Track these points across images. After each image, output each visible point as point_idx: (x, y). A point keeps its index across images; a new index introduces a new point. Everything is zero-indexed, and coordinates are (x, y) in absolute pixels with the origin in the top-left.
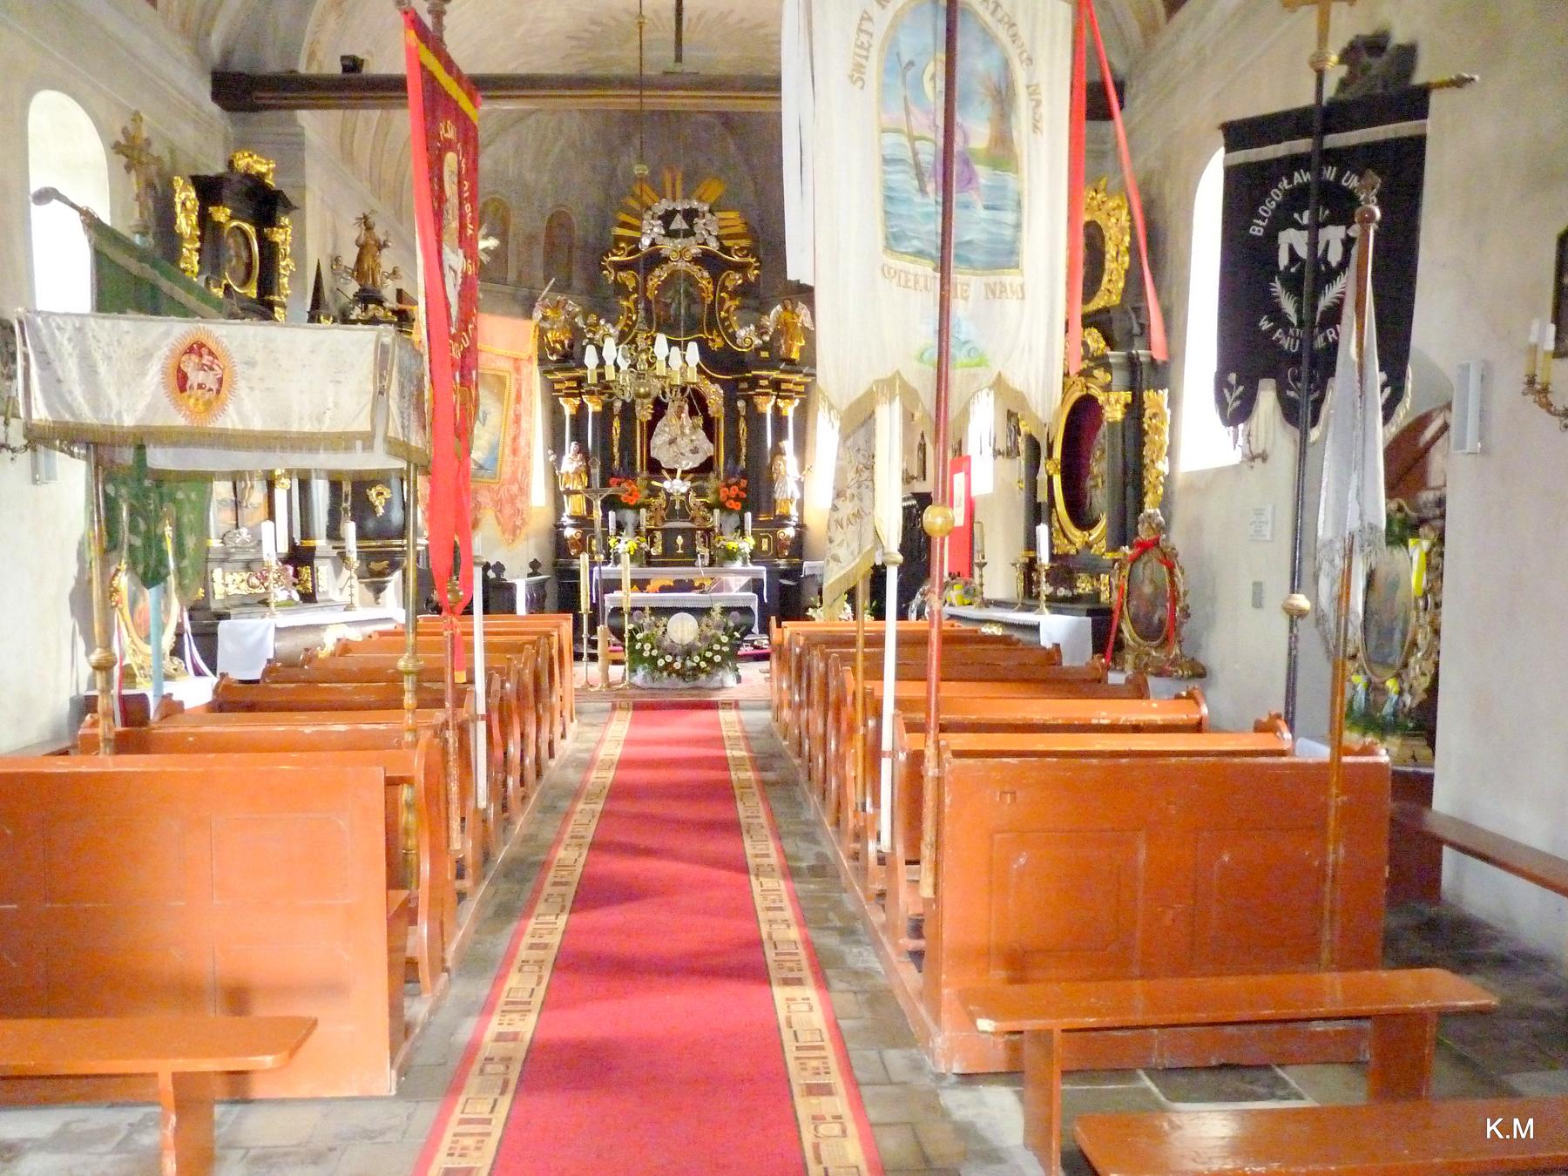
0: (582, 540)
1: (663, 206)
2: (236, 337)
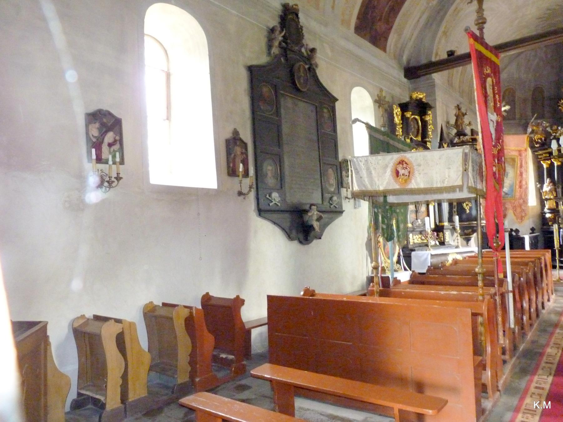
0: (554, 218)
2: (415, 156)
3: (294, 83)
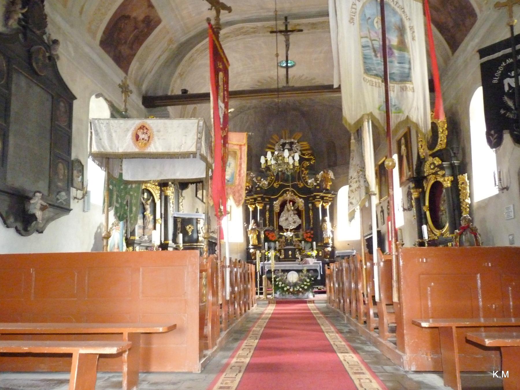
1: (282, 141)
3: (31, 64)
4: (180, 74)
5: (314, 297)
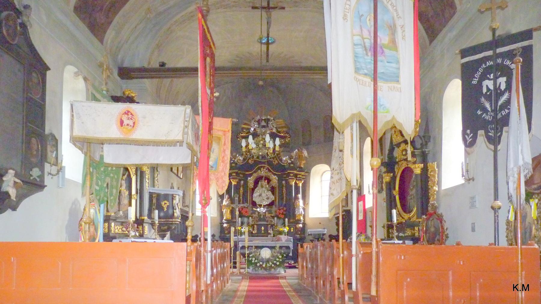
4: (158, 45)
5: (285, 272)
